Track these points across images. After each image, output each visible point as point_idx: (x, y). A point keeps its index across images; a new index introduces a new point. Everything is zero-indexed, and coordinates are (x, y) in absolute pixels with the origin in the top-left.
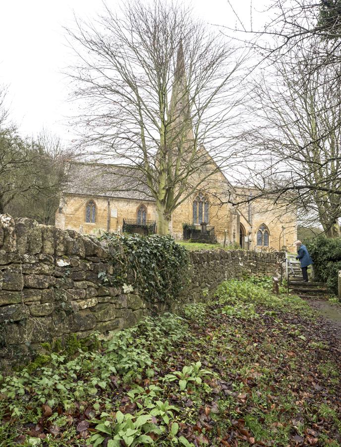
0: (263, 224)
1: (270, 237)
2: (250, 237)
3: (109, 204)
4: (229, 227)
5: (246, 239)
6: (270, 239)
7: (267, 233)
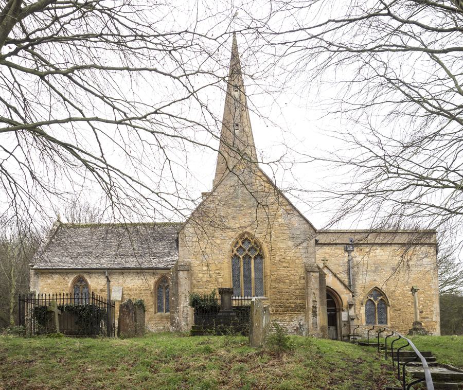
0: (376, 289)
1: (388, 308)
2: (352, 312)
3: (109, 281)
4: (304, 297)
5: (344, 316)
6: (390, 313)
7: (384, 304)
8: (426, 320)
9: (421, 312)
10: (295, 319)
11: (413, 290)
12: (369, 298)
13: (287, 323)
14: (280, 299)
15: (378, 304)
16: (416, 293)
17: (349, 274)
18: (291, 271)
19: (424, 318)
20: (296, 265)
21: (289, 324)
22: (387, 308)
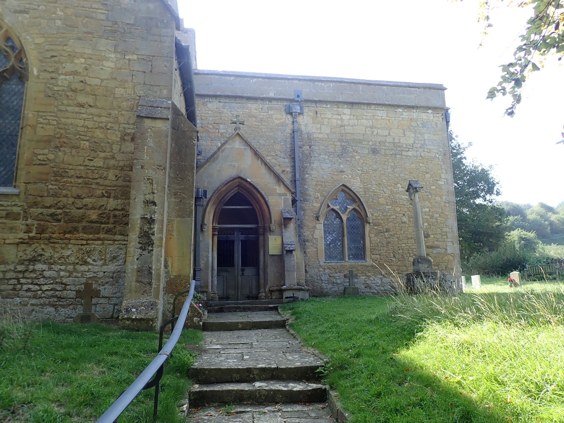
0: (345, 189)
8: (435, 251)
9: (427, 236)
10: (96, 256)
11: (412, 189)
12: (332, 207)
13: (70, 268)
14: (55, 195)
15: (348, 219)
16: (417, 195)
17: (294, 159)
18: (100, 116)
19: (431, 247)
20: (115, 104)
21: (75, 270)
22: (364, 227)
